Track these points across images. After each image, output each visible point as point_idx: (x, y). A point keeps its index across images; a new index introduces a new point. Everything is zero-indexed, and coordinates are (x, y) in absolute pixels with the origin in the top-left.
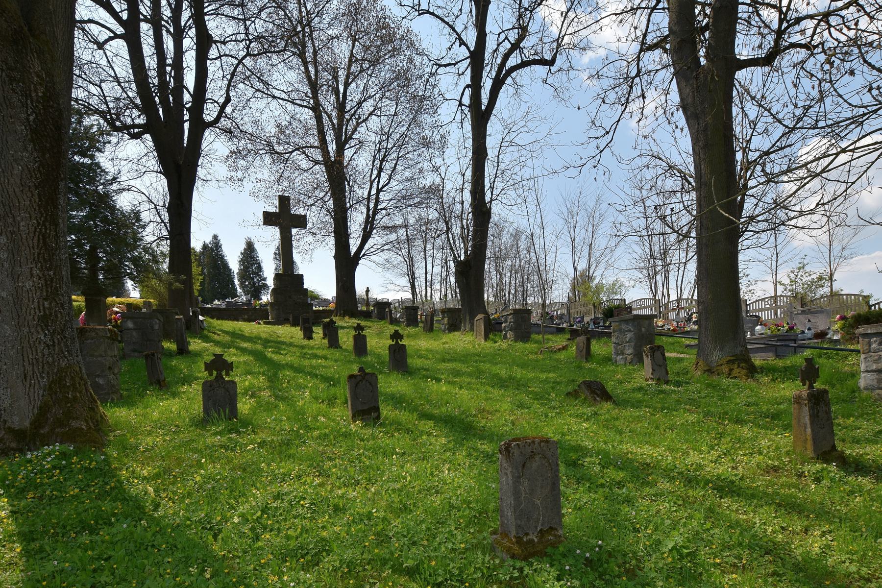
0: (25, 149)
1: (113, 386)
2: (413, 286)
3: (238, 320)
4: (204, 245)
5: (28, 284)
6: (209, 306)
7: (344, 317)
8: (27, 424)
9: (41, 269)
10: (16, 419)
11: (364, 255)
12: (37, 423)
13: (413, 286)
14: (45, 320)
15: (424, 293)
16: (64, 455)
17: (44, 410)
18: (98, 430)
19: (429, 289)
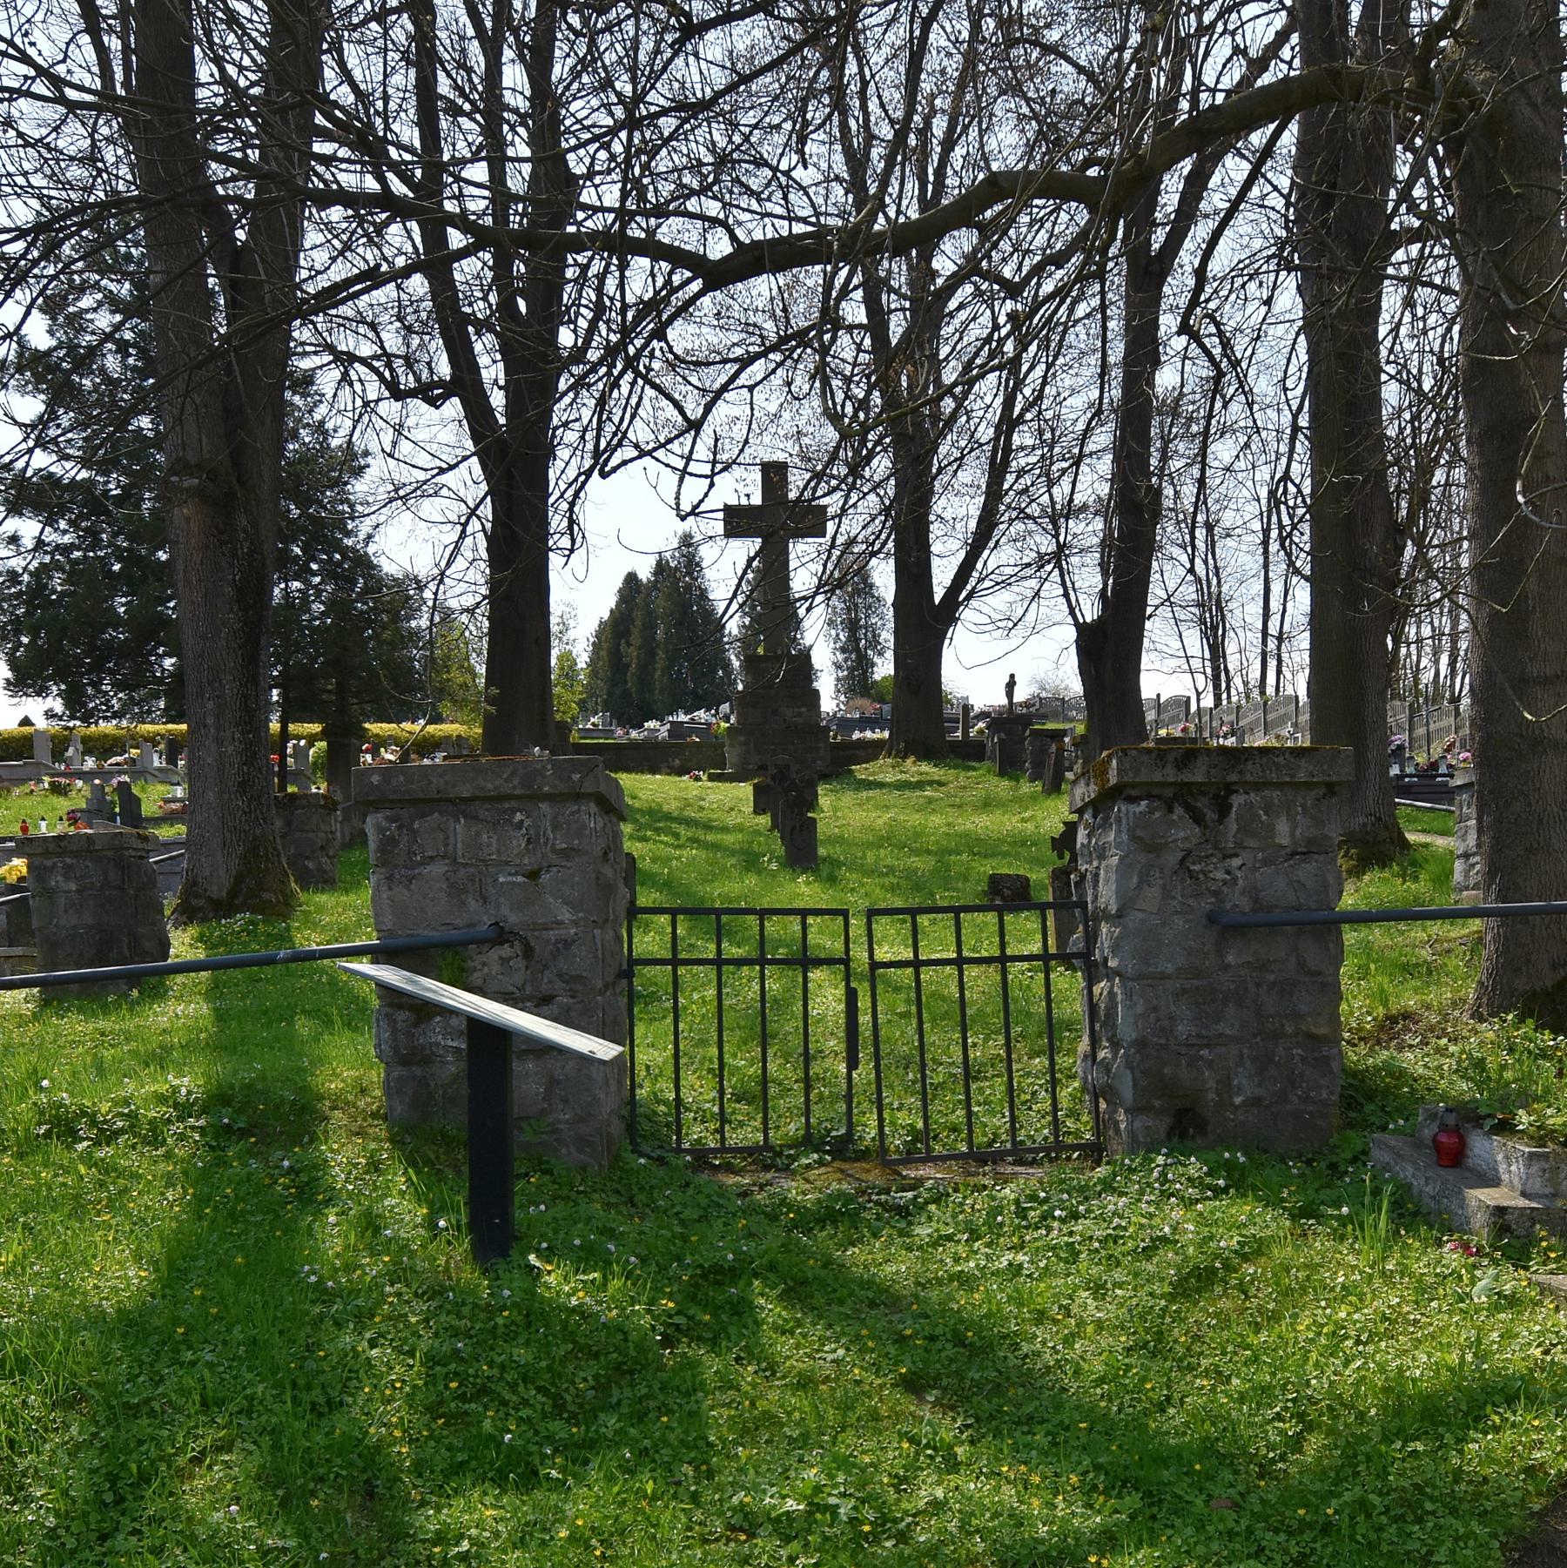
0: (232, 610)
1: (325, 872)
2: (1217, 652)
3: (654, 771)
4: (659, 563)
5: (230, 749)
6: (426, 762)
7: (904, 758)
8: (224, 894)
9: (242, 733)
10: (215, 888)
11: (970, 597)
12: (233, 893)
13: (1217, 652)
14: (243, 786)
15: (1255, 674)
16: (252, 922)
17: (239, 879)
18: (287, 904)
19: (1272, 664)
